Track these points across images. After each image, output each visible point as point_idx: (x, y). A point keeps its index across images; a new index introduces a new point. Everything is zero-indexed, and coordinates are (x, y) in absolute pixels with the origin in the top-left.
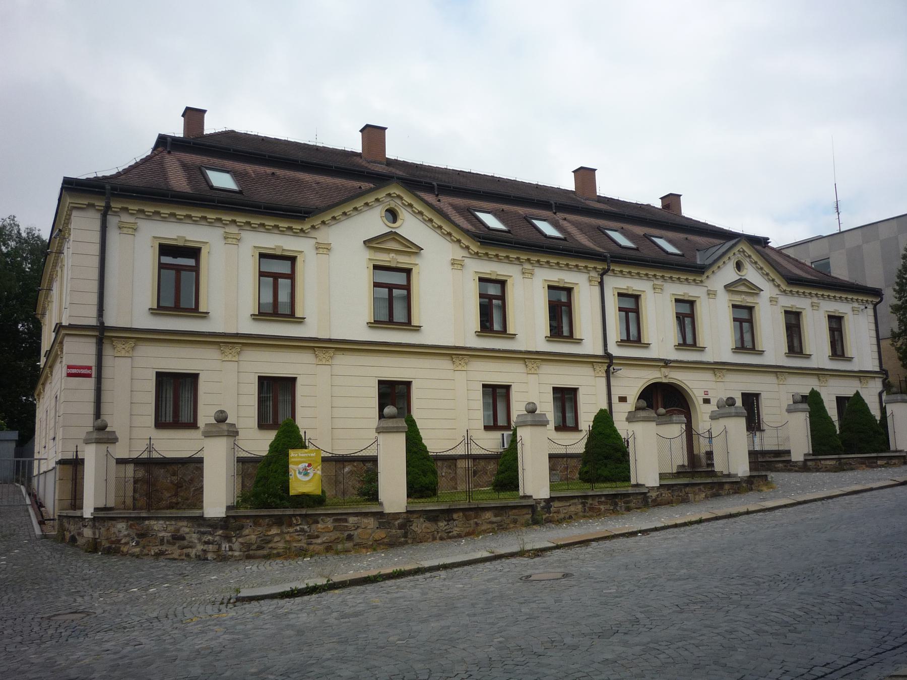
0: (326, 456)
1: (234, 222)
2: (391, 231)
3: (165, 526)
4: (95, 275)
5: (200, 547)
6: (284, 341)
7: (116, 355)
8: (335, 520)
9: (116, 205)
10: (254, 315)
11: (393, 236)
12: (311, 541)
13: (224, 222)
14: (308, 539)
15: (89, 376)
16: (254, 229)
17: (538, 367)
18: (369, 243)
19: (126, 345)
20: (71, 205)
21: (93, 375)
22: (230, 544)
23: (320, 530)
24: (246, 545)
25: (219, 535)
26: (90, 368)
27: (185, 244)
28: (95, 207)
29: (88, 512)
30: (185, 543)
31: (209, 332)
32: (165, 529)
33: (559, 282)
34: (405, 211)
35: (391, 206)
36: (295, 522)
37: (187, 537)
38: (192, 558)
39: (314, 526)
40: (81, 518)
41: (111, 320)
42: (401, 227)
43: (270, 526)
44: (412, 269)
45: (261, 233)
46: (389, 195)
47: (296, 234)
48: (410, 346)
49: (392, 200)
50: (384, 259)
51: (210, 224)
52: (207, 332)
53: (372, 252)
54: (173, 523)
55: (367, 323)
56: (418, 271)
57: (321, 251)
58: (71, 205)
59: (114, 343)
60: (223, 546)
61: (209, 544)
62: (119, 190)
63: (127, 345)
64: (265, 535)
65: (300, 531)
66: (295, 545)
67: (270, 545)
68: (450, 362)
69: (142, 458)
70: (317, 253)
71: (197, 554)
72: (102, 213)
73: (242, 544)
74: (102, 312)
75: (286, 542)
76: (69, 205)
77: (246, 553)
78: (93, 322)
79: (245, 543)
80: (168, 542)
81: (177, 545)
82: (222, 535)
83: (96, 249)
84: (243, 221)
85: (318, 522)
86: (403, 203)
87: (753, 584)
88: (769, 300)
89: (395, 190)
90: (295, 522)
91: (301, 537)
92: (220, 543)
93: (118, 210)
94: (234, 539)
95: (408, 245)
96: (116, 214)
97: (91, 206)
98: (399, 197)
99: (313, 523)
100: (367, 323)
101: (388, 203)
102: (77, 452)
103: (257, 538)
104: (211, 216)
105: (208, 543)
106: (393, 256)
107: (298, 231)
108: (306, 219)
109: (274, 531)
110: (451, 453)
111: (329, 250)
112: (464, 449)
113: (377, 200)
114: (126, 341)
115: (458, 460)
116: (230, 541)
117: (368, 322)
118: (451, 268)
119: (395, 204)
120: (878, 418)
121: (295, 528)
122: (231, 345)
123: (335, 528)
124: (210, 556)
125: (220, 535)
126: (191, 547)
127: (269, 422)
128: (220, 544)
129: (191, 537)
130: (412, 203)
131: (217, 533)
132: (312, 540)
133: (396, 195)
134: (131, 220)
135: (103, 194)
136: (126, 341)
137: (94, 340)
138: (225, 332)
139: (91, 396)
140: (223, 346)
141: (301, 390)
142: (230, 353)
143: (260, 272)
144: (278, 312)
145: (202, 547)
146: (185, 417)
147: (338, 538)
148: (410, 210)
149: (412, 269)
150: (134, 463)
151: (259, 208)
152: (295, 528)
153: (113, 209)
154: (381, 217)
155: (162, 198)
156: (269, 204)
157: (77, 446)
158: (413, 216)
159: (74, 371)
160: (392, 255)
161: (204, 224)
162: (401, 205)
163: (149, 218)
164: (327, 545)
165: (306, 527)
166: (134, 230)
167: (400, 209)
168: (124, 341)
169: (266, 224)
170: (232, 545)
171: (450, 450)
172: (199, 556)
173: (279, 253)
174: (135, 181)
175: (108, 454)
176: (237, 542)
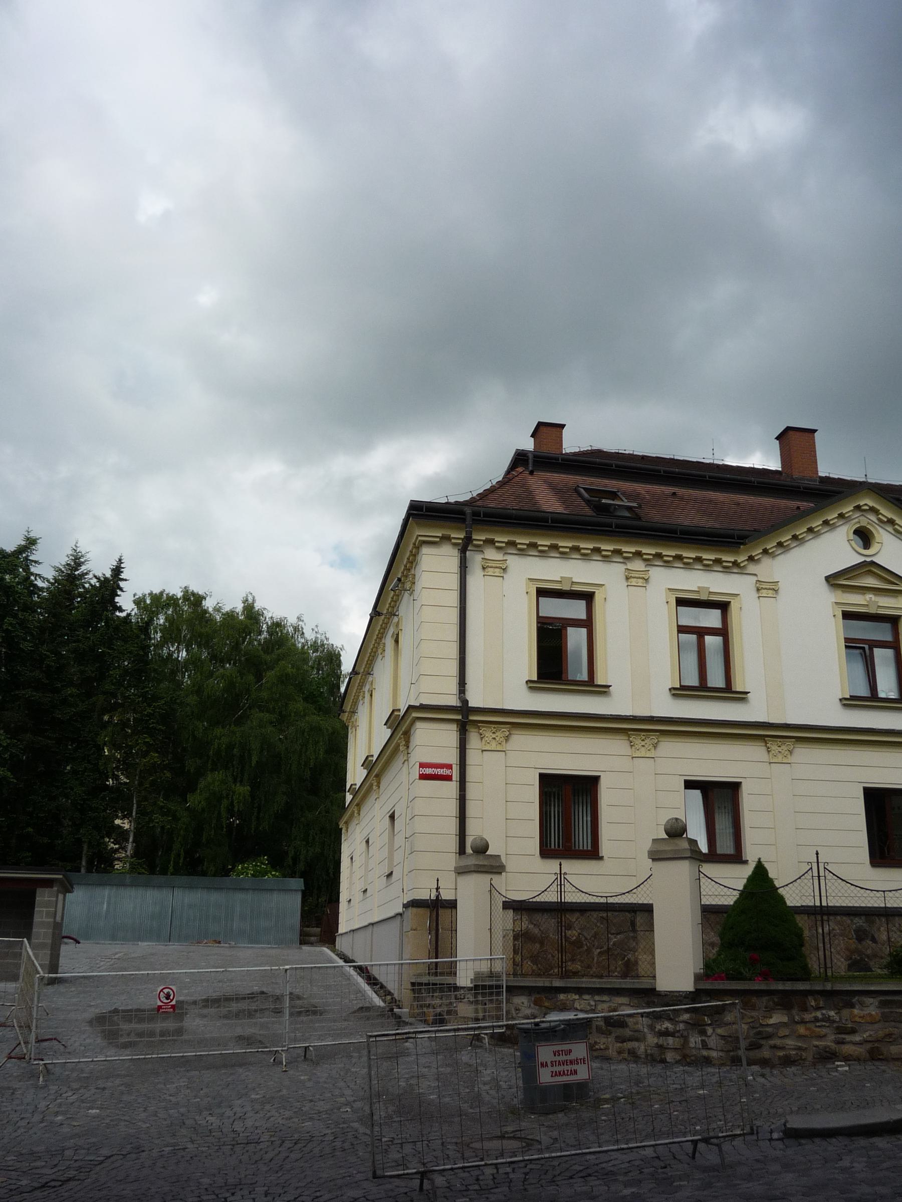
0: (592, 901)
1: (638, 554)
2: (865, 561)
3: (593, 1003)
4: (453, 634)
5: (652, 1040)
6: (529, 718)
7: (771, 761)
8: (883, 1004)
9: (479, 537)
10: (675, 689)
11: (869, 567)
12: (844, 1039)
13: (645, 557)
14: (837, 1033)
15: (448, 778)
16: (667, 564)
17: (791, 752)
18: (834, 580)
19: (497, 734)
20: (420, 538)
21: (454, 778)
22: (704, 1038)
23: (857, 1019)
24: (730, 1039)
25: (683, 1022)
26: (449, 767)
27: (572, 589)
28: (451, 540)
29: (464, 978)
30: (627, 1032)
31: (611, 715)
32: (593, 1008)
33: (698, 592)
34: (885, 532)
35: (863, 524)
36: (813, 1003)
37: (630, 1021)
38: (640, 1058)
39: (846, 1012)
40: (456, 988)
41: (474, 701)
42: (881, 552)
43: (769, 1011)
44: (594, 593)
45: (716, 573)
46: (858, 508)
47: (727, 570)
48: (620, 719)
49: (862, 515)
50: (858, 601)
51: (606, 559)
52: (608, 715)
53: (839, 592)
54: (605, 998)
55: (841, 700)
56: (604, 597)
57: (764, 593)
58: (420, 538)
59: (631, 739)
60: (692, 1040)
61: (669, 1036)
62: (424, 511)
63: (784, 747)
64: (762, 1025)
65: (822, 1020)
66: (817, 1043)
67: (772, 1042)
68: (626, 743)
69: (537, 902)
70: (759, 597)
71: (649, 1051)
72: (460, 548)
73: (723, 1037)
74: (464, 687)
75: (800, 1037)
76: (417, 538)
77: (732, 1054)
78: (453, 701)
79: (730, 1037)
80: (599, 1030)
81: (613, 1035)
82: (690, 1021)
83: (453, 598)
84: (651, 553)
85: (852, 1006)
86: (880, 520)
87: (820, 1166)
88: (756, 589)
89: (867, 501)
90: (813, 1003)
91: (824, 1031)
92: (685, 1033)
93: (691, 561)
94: (710, 1031)
95: (895, 581)
96: (479, 549)
97: (446, 539)
98: (873, 510)
99: (844, 1007)
100: (841, 700)
101: (857, 520)
102: (437, 889)
103: (748, 1029)
104: (689, 554)
105: (666, 1033)
106: (871, 598)
107: (731, 565)
108: (742, 547)
109: (777, 1018)
110: (538, 900)
111: (776, 591)
112: (811, 891)
113: (841, 516)
114: (647, 735)
115: (638, 913)
116: (703, 1033)
117: (841, 697)
118: (483, 574)
119: (868, 521)
120: (346, 806)
121: (813, 1014)
122: (645, 734)
123: (885, 1018)
124: (670, 1056)
125: (686, 1022)
126: (637, 1040)
127: (550, 846)
128: (686, 1037)
129: (636, 1023)
130: (894, 518)
131: (681, 1018)
132: (843, 1036)
133: (868, 508)
134: (499, 556)
135: (463, 521)
136: (647, 735)
137: (454, 727)
138: (634, 715)
139: (452, 807)
140: (633, 735)
141: (606, 796)
142: (643, 746)
143: (678, 626)
144: (707, 684)
145: (656, 1040)
146: (584, 842)
147: (890, 1035)
148: (890, 529)
149: (594, 593)
150: (514, 910)
151: (546, 522)
152: (813, 1014)
153: (475, 542)
154: (848, 541)
155: (526, 522)
156: (710, 529)
157: (438, 880)
158: (896, 539)
159: (429, 771)
160: (869, 596)
161: (619, 560)
162: (877, 522)
163: (522, 553)
164: (869, 1046)
165: (832, 1013)
166: (775, 592)
167: (876, 529)
168: (780, 742)
169: (704, 557)
170: (706, 1039)
171: (543, 892)
172: (651, 1055)
173: (566, 587)
174: (492, 504)
175: (494, 892)
176: (714, 1035)
